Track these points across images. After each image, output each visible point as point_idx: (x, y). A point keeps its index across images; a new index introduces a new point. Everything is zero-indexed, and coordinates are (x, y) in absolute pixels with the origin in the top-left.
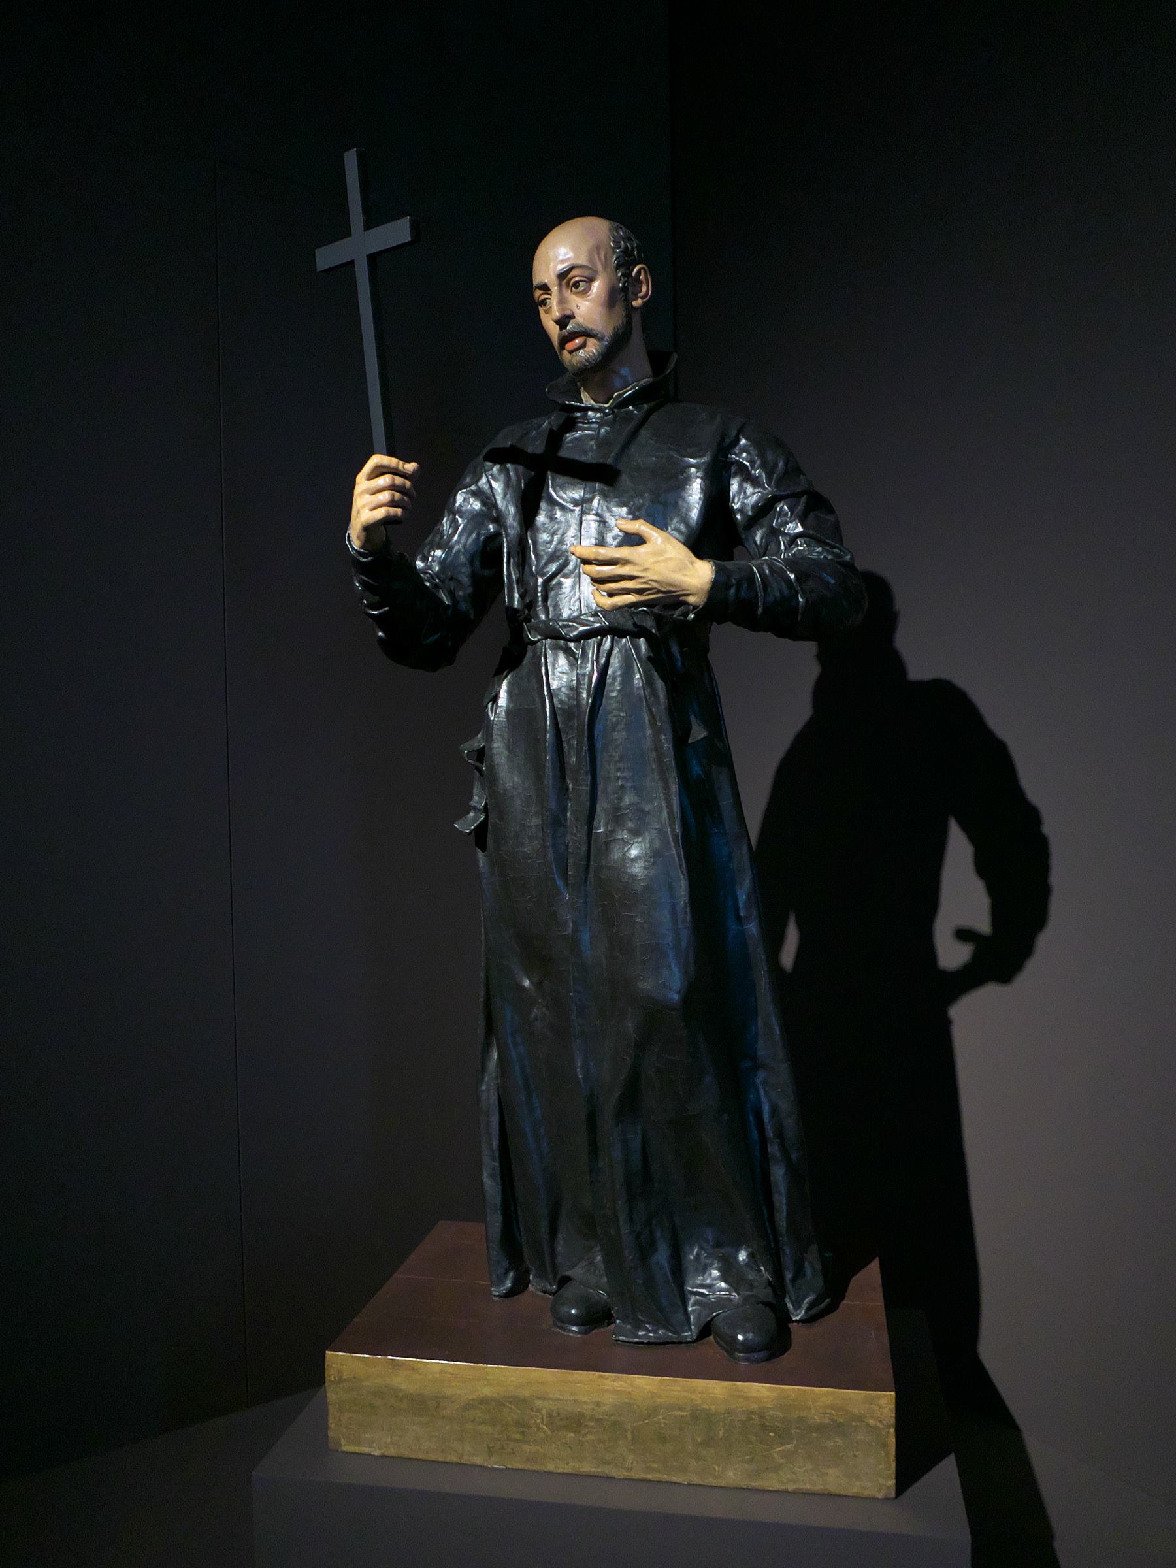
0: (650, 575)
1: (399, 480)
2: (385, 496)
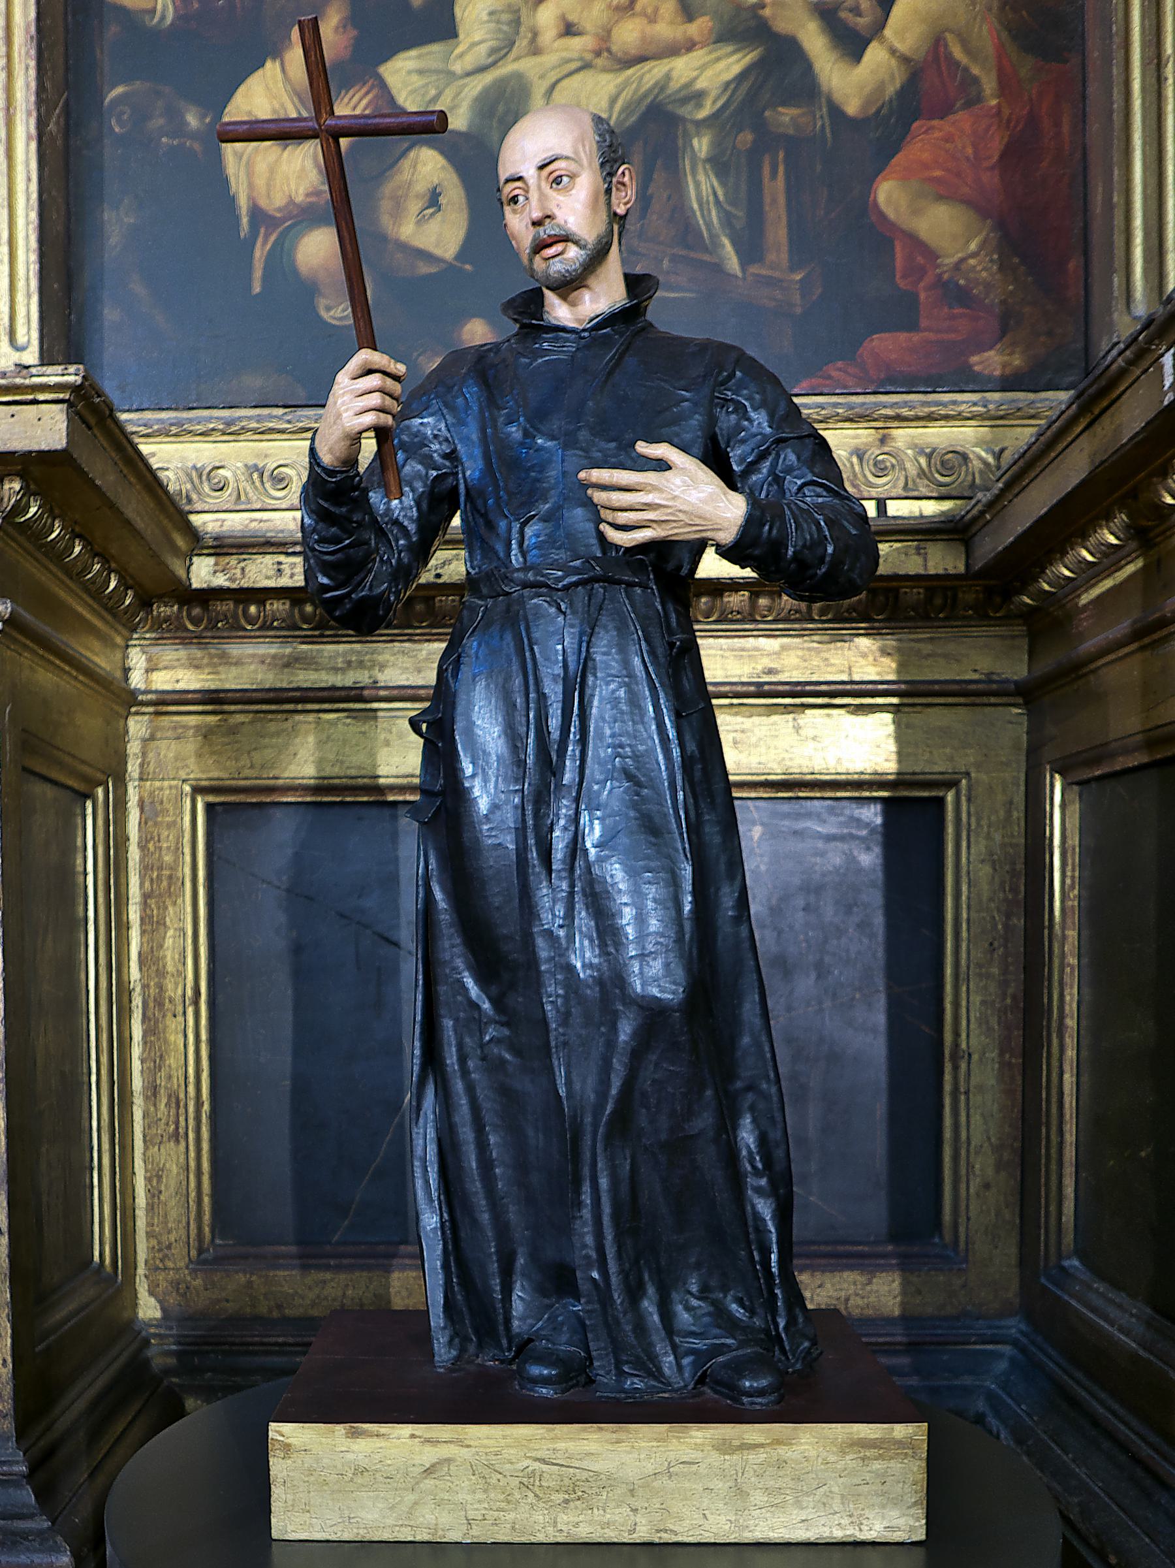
0: (678, 504)
1: (389, 382)
2: (375, 399)
